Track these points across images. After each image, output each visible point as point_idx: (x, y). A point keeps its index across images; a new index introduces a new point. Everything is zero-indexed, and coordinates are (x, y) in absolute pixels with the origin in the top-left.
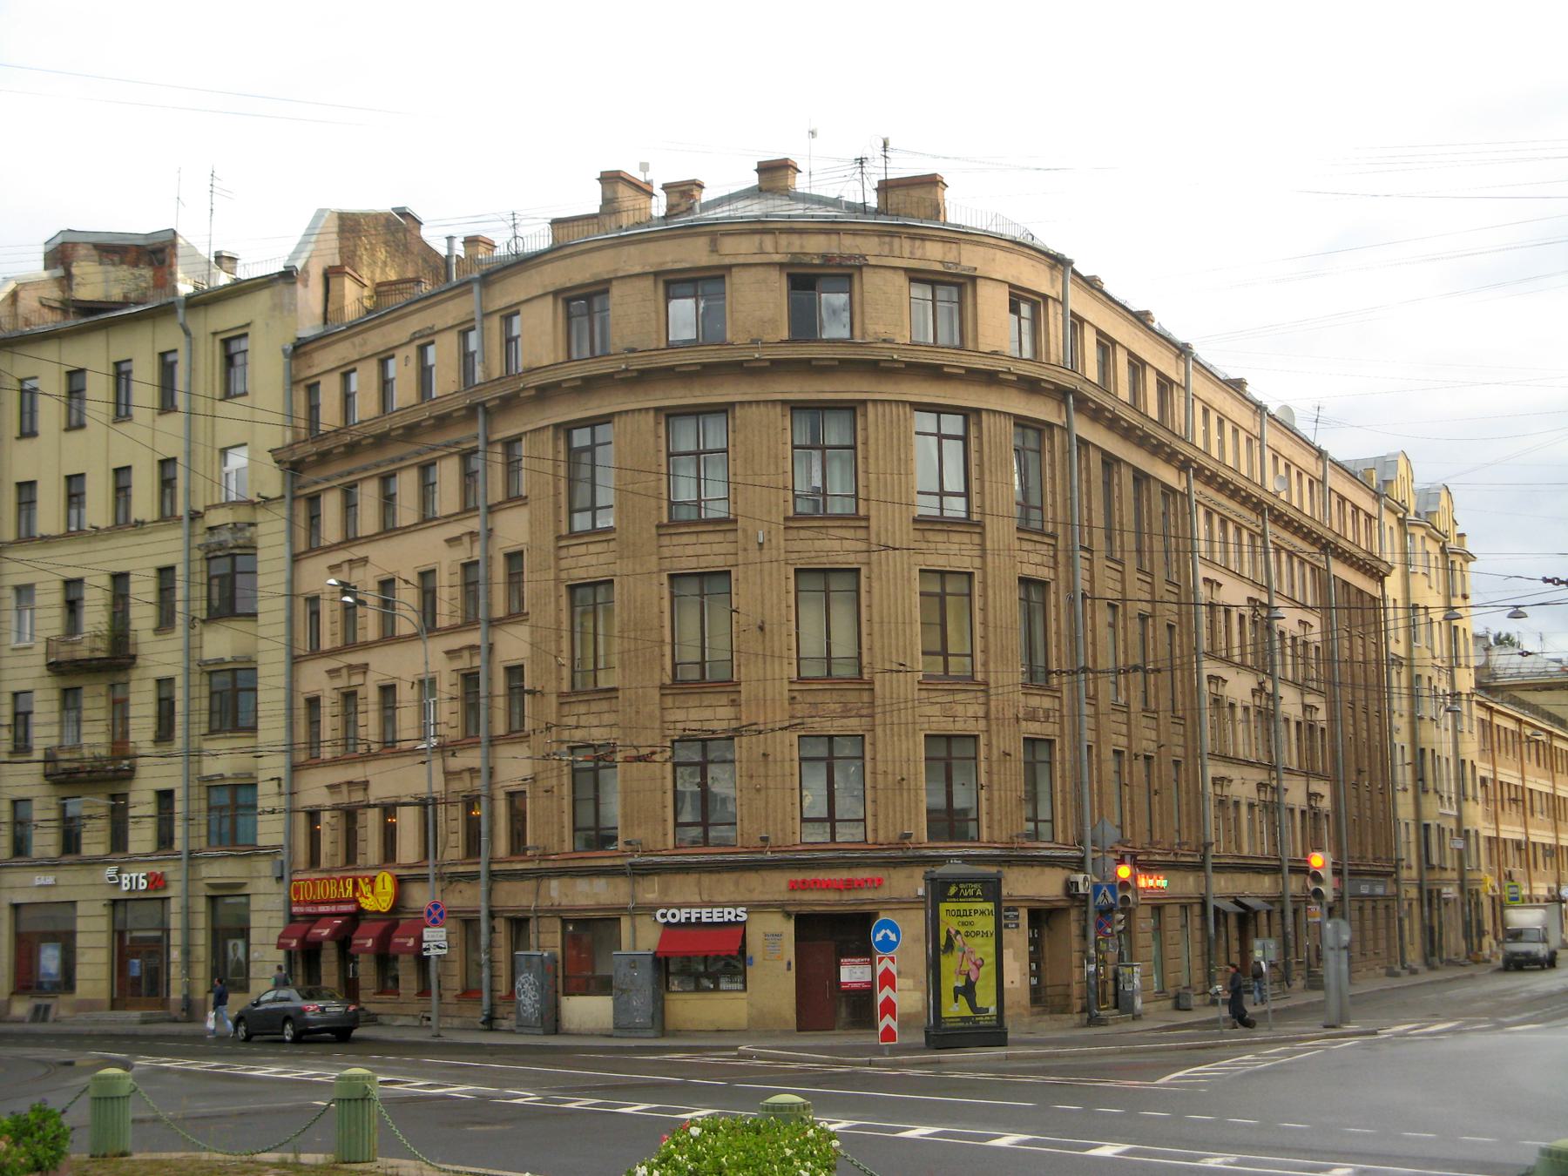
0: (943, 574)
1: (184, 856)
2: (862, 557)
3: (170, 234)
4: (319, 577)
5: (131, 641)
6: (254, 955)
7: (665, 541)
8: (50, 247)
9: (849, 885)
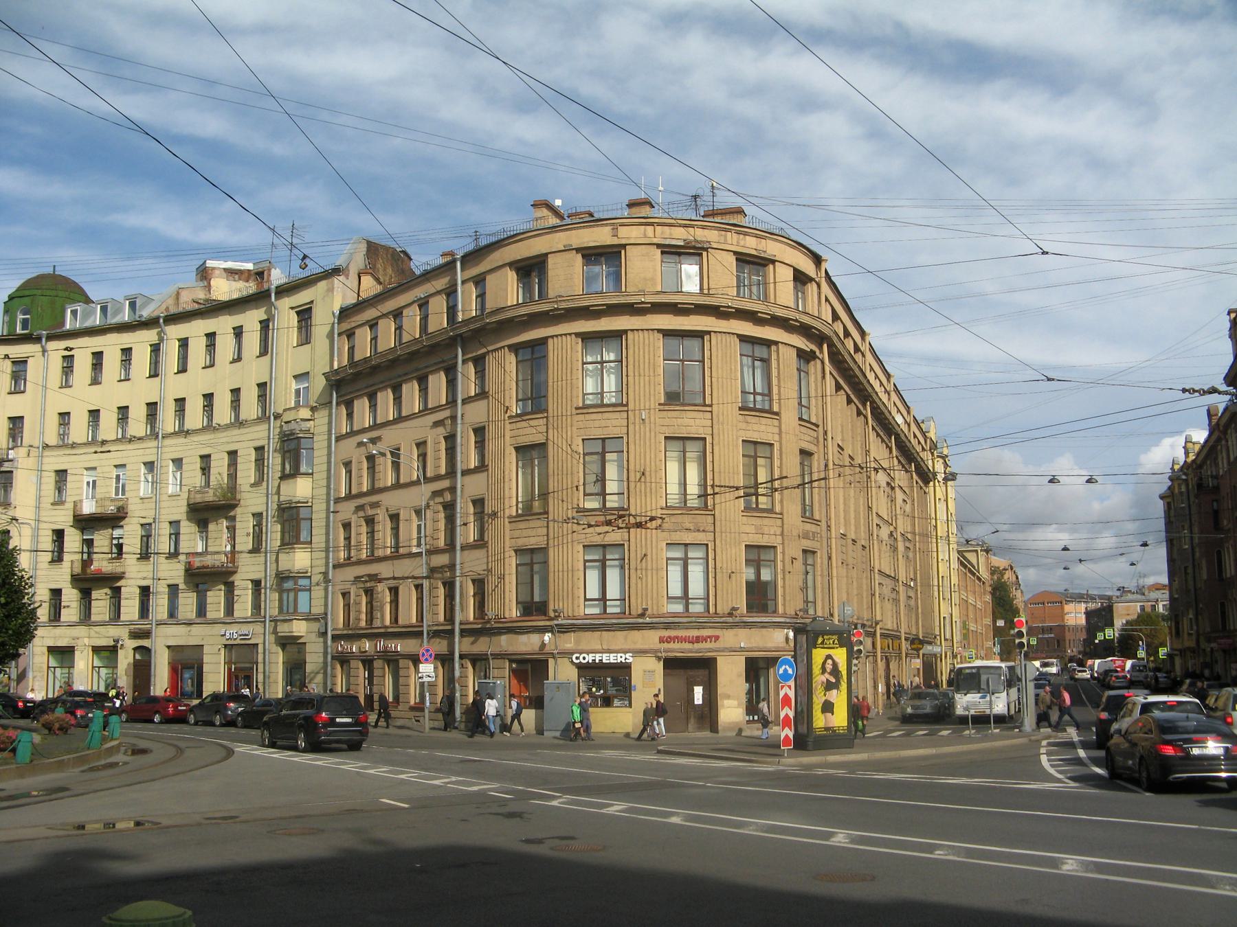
0: (755, 443)
9: (698, 640)
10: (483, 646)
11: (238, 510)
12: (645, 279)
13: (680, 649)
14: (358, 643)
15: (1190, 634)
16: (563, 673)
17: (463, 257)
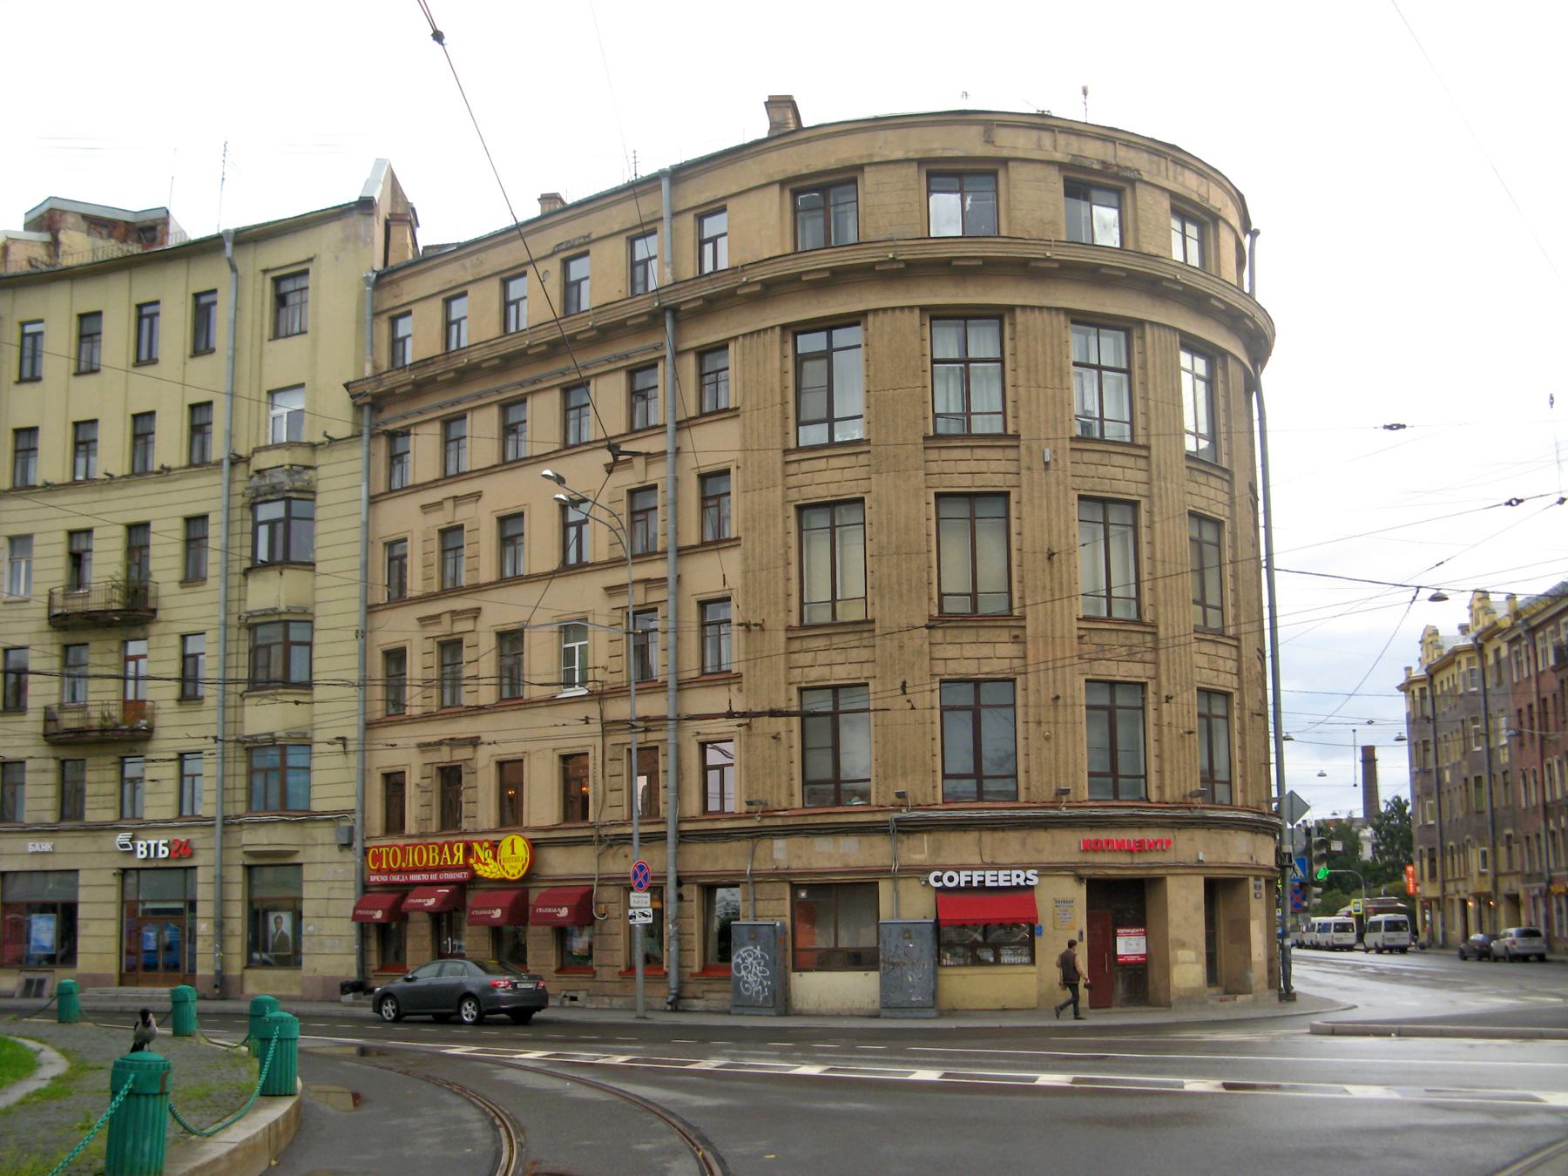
1: (218, 822)
2: (1142, 489)
3: (163, 214)
4: (406, 518)
5: (151, 594)
6: (308, 927)
7: (933, 454)
8: (32, 216)
9: (1140, 847)
13: (1114, 863)
15: (1482, 874)
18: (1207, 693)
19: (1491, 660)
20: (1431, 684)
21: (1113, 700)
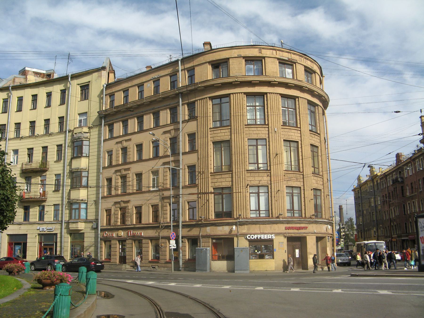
9: (300, 228)
10: (195, 232)
11: (47, 173)
12: (273, 72)
13: (294, 233)
14: (117, 232)
15: (374, 236)
16: (241, 244)
17: (182, 59)
18: (315, 189)
19: (375, 183)
20: (360, 189)
21: (293, 191)
